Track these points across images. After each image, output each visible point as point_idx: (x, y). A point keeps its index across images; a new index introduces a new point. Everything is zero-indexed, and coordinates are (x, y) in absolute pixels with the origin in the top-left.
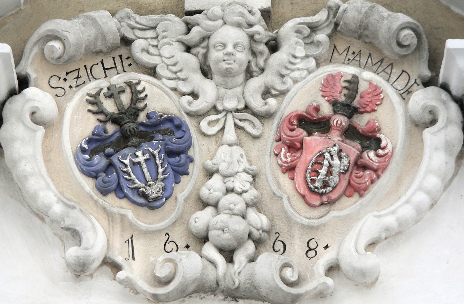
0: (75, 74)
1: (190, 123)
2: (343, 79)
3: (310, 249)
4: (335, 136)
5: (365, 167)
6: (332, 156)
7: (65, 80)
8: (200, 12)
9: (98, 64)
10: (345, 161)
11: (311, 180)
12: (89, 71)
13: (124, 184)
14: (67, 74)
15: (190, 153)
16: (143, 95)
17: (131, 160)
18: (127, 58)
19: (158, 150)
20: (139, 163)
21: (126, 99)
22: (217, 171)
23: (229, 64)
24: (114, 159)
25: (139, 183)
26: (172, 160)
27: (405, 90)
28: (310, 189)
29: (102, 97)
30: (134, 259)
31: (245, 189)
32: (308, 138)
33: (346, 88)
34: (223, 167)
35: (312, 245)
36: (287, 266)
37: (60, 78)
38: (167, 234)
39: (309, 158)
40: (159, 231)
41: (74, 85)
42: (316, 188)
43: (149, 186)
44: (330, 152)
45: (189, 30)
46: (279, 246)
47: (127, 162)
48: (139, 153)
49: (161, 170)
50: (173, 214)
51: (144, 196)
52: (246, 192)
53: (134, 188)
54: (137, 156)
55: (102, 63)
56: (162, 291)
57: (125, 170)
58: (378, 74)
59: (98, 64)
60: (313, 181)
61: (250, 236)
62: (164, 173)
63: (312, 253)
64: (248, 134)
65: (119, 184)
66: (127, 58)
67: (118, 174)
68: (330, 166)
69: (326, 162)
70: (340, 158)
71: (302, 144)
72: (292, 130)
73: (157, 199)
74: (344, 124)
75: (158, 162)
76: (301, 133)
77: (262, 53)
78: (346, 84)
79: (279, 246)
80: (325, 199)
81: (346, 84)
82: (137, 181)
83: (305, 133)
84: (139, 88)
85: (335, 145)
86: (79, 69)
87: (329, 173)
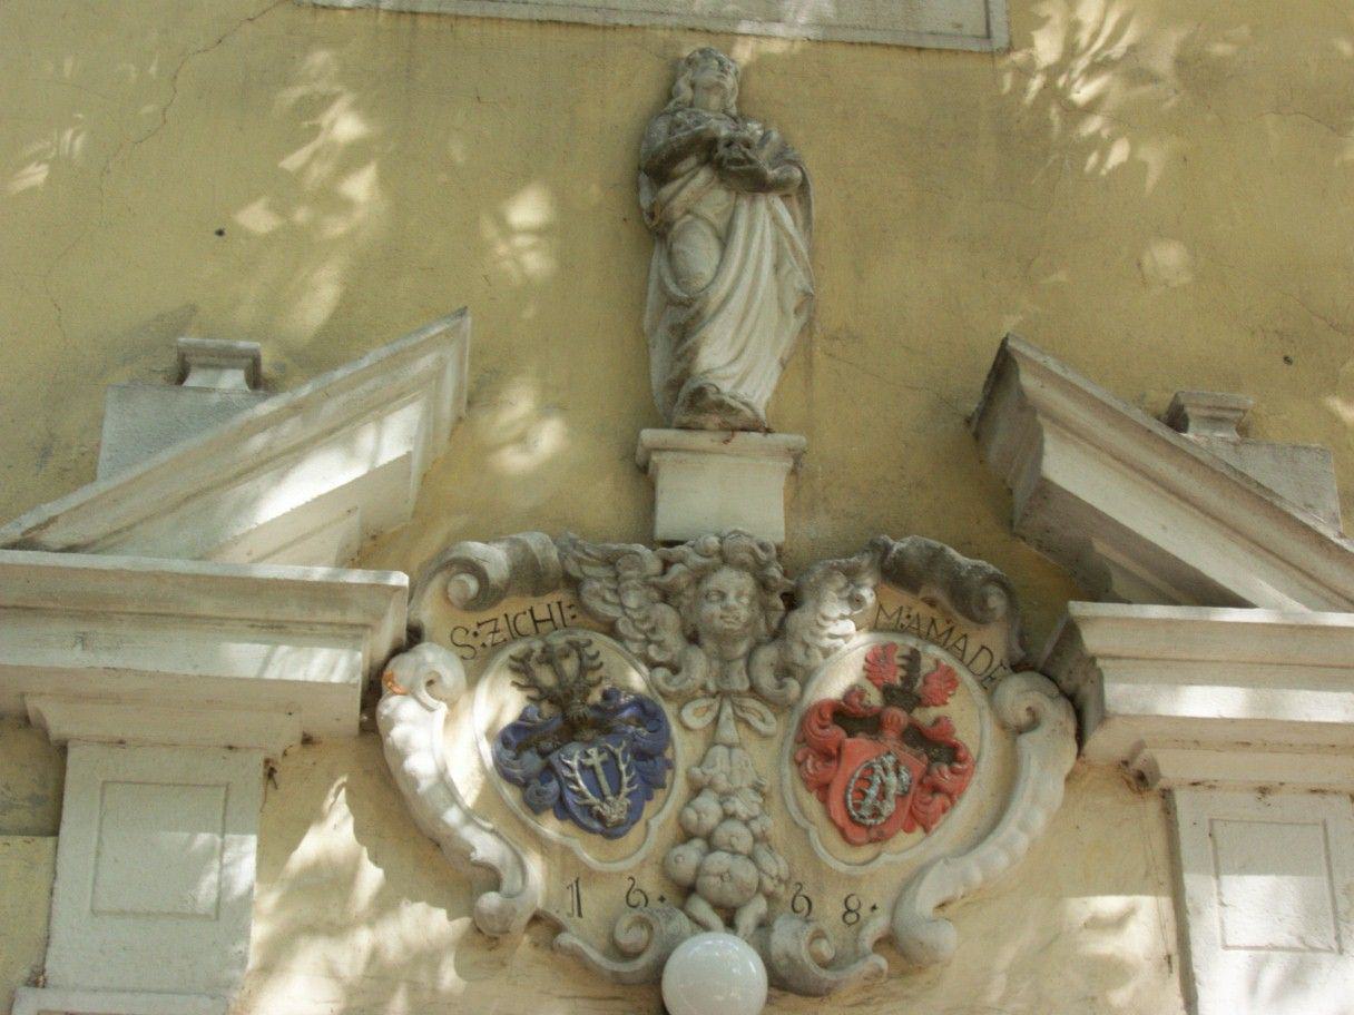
0: (490, 627)
1: (669, 709)
2: (898, 653)
3: (849, 911)
4: (890, 739)
5: (936, 789)
6: (885, 770)
7: (476, 634)
8: (682, 543)
9: (525, 613)
10: (905, 776)
11: (854, 804)
12: (511, 624)
13: (570, 798)
14: (479, 625)
15: (668, 754)
16: (596, 663)
17: (580, 763)
18: (570, 607)
19: (621, 749)
20: (592, 767)
21: (570, 666)
22: (711, 785)
23: (729, 623)
24: (553, 758)
25: (593, 799)
26: (642, 764)
27: (986, 675)
28: (851, 818)
29: (532, 664)
30: (580, 915)
31: (752, 814)
32: (849, 741)
33: (902, 667)
34: (722, 783)
35: (853, 904)
36: (818, 937)
37: (467, 632)
38: (633, 879)
39: (850, 771)
40: (620, 874)
41: (488, 642)
42: (862, 817)
43: (608, 803)
44: (882, 763)
45: (664, 572)
46: (801, 904)
47: (574, 764)
48: (593, 751)
49: (625, 779)
50: (61, 671)
51: (600, 818)
52: (755, 818)
53: (586, 805)
54: (588, 756)
55: (531, 611)
56: (624, 968)
57: (570, 775)
58: (947, 649)
59: (525, 613)
60: (857, 807)
61: (760, 888)
62: (630, 784)
63: (851, 917)
64: (757, 732)
65: (561, 798)
66: (570, 607)
67: (560, 782)
68: (883, 784)
69: (877, 780)
70: (898, 773)
71: (839, 750)
72: (823, 727)
73: (619, 824)
74: (902, 722)
75: (623, 767)
76: (837, 732)
77: (775, 609)
78: (903, 662)
79: (801, 904)
80: (874, 834)
81: (903, 662)
82: (581, 783)
83: (843, 733)
84: (591, 651)
85: (889, 753)
86: (496, 619)
87: (883, 795)
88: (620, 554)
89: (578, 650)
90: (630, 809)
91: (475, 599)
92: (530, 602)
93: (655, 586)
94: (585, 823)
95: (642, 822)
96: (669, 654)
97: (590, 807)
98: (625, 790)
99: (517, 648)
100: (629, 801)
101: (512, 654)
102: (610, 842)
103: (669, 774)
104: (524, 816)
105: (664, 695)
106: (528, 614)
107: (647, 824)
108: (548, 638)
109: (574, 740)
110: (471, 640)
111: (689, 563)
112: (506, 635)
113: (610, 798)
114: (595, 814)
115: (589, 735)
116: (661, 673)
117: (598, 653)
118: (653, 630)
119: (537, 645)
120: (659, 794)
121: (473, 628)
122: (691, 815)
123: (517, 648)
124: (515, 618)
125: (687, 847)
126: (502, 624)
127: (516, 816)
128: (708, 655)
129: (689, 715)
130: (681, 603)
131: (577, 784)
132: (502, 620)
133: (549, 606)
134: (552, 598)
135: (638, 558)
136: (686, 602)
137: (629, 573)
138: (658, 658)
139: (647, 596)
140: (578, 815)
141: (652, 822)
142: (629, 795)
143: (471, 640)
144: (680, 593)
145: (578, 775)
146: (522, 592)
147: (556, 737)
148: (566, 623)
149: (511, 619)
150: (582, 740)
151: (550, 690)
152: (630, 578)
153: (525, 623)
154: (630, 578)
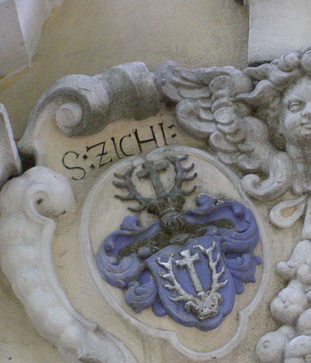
0: (99, 149)
7: (85, 157)
13: (165, 297)
14: (88, 149)
15: (257, 252)
16: (191, 174)
17: (173, 263)
20: (185, 267)
22: (295, 276)
24: (151, 263)
25: (184, 295)
29: (134, 179)
43: (200, 298)
49: (216, 276)
51: (193, 312)
53: (179, 302)
55: (136, 133)
59: (130, 135)
62: (220, 280)
66: (170, 127)
73: (211, 316)
75: (213, 265)
82: (183, 292)
84: (187, 165)
86: (104, 143)
88: (212, 76)
89: (173, 163)
90: (221, 303)
91: (79, 125)
92: (134, 125)
93: (243, 101)
94: (180, 317)
95: (233, 314)
96: (258, 162)
97: (183, 302)
98: (216, 285)
99: (122, 166)
100: (219, 296)
101: (115, 172)
102: (205, 333)
103: (258, 269)
104: (126, 316)
105: (252, 198)
106: (133, 136)
107: (238, 315)
108: (148, 155)
109: (169, 244)
110: (80, 162)
111: (272, 78)
112: (113, 155)
113: (201, 293)
114: (188, 309)
115: (183, 237)
116: (250, 179)
117: (193, 166)
118: (243, 141)
119: (138, 162)
120: (249, 288)
121: (83, 152)
122: (277, 304)
123: (122, 166)
124: (121, 140)
125: (276, 333)
126: (109, 147)
127: (118, 315)
128: (291, 159)
129: (275, 215)
130: (268, 115)
131: (178, 294)
132: (109, 143)
133: (152, 127)
134: (154, 121)
135: (228, 77)
136: (272, 114)
137: (220, 92)
138: (248, 167)
139: (236, 111)
140: (174, 312)
141: (242, 314)
142: (218, 291)
143: (80, 162)
144: (267, 106)
145: (177, 285)
146: (125, 117)
147: (154, 243)
148: (167, 142)
149: (117, 141)
150: (176, 243)
151: (148, 200)
152: (222, 96)
153: (130, 144)
154: (222, 96)
